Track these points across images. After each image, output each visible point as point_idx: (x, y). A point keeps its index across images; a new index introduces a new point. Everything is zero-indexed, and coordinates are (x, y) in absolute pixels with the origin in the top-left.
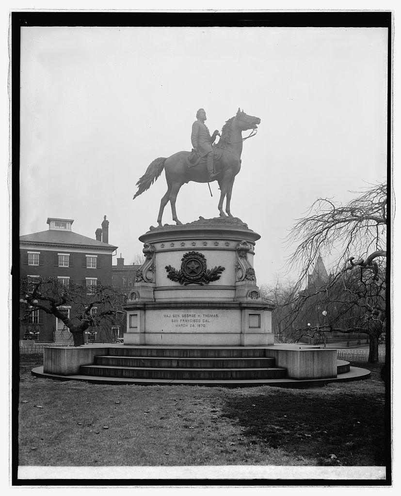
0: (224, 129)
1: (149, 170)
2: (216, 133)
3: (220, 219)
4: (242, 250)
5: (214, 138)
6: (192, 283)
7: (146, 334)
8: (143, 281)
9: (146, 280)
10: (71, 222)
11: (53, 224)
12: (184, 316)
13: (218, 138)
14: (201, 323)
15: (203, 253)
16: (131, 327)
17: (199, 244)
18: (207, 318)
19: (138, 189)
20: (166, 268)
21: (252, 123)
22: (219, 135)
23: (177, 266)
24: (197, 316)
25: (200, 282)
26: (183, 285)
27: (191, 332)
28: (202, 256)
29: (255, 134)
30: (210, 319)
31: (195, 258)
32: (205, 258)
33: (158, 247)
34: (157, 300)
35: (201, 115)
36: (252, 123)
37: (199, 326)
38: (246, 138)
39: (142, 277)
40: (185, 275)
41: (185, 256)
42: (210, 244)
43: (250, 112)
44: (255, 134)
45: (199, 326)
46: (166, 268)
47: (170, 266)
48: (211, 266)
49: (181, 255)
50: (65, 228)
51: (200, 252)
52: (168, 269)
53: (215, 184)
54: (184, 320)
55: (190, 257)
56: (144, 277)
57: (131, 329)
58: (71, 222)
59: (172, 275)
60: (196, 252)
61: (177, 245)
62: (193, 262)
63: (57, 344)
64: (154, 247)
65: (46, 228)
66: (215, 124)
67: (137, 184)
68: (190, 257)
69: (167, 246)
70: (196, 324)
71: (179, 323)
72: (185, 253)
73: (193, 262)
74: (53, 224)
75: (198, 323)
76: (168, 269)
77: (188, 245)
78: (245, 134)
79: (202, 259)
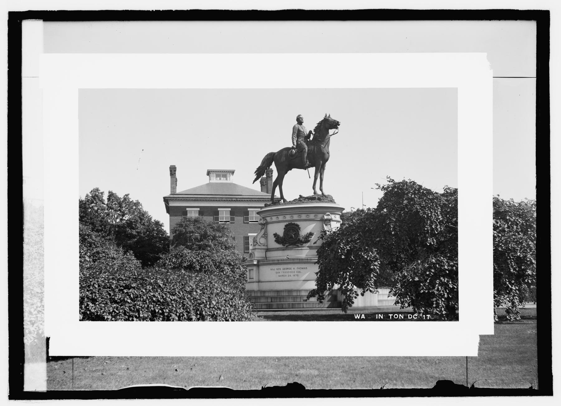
0: (315, 130)
1: (263, 162)
2: (310, 132)
3: (314, 196)
4: (327, 220)
5: (309, 136)
6: (291, 245)
7: (260, 283)
8: (258, 245)
9: (260, 244)
10: (233, 172)
11: (213, 176)
12: (284, 269)
13: (312, 137)
14: (296, 273)
15: (298, 223)
16: (250, 278)
17: (296, 217)
18: (299, 270)
19: (256, 177)
20: (274, 235)
21: (335, 125)
22: (313, 134)
23: (281, 233)
24: (292, 269)
25: (297, 244)
26: (285, 247)
27: (280, 280)
28: (298, 226)
29: (337, 132)
30: (302, 271)
31: (293, 228)
32: (300, 227)
33: (268, 219)
34: (268, 258)
35: (300, 121)
36: (335, 125)
37: (294, 275)
38: (331, 135)
39: (257, 243)
40: (286, 240)
41: (286, 226)
42: (304, 217)
43: (334, 117)
44: (337, 132)
45: (294, 275)
46: (274, 235)
47: (276, 233)
48: (303, 232)
49: (282, 226)
50: (226, 179)
51: (296, 223)
52: (275, 235)
53: (312, 170)
54: (284, 272)
55: (289, 227)
56: (258, 243)
57: (250, 280)
58: (233, 172)
59: (278, 239)
60: (293, 223)
61: (281, 218)
62: (291, 230)
63: (329, 287)
64: (266, 219)
65: (206, 180)
66: (309, 126)
67: (255, 172)
68: (289, 227)
69: (274, 219)
70: (292, 274)
71: (281, 274)
72: (286, 223)
73: (291, 230)
74: (213, 176)
75: (294, 274)
76: (275, 235)
77: (288, 218)
78: (331, 131)
79: (297, 227)
